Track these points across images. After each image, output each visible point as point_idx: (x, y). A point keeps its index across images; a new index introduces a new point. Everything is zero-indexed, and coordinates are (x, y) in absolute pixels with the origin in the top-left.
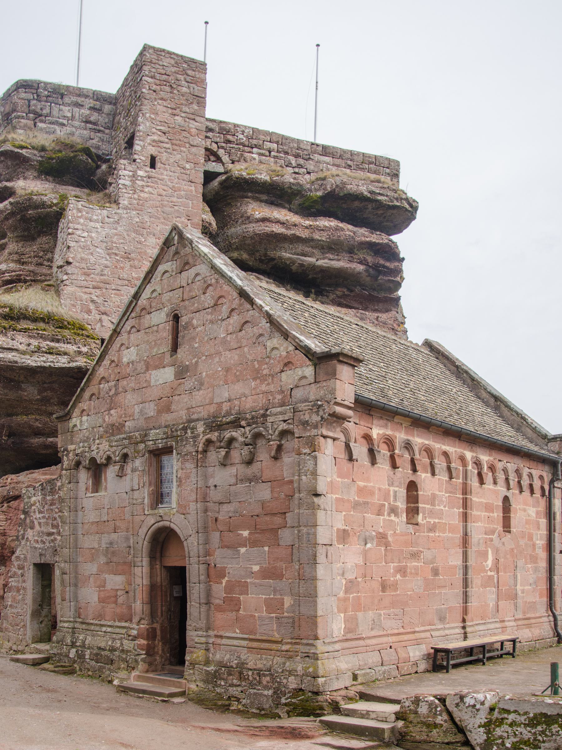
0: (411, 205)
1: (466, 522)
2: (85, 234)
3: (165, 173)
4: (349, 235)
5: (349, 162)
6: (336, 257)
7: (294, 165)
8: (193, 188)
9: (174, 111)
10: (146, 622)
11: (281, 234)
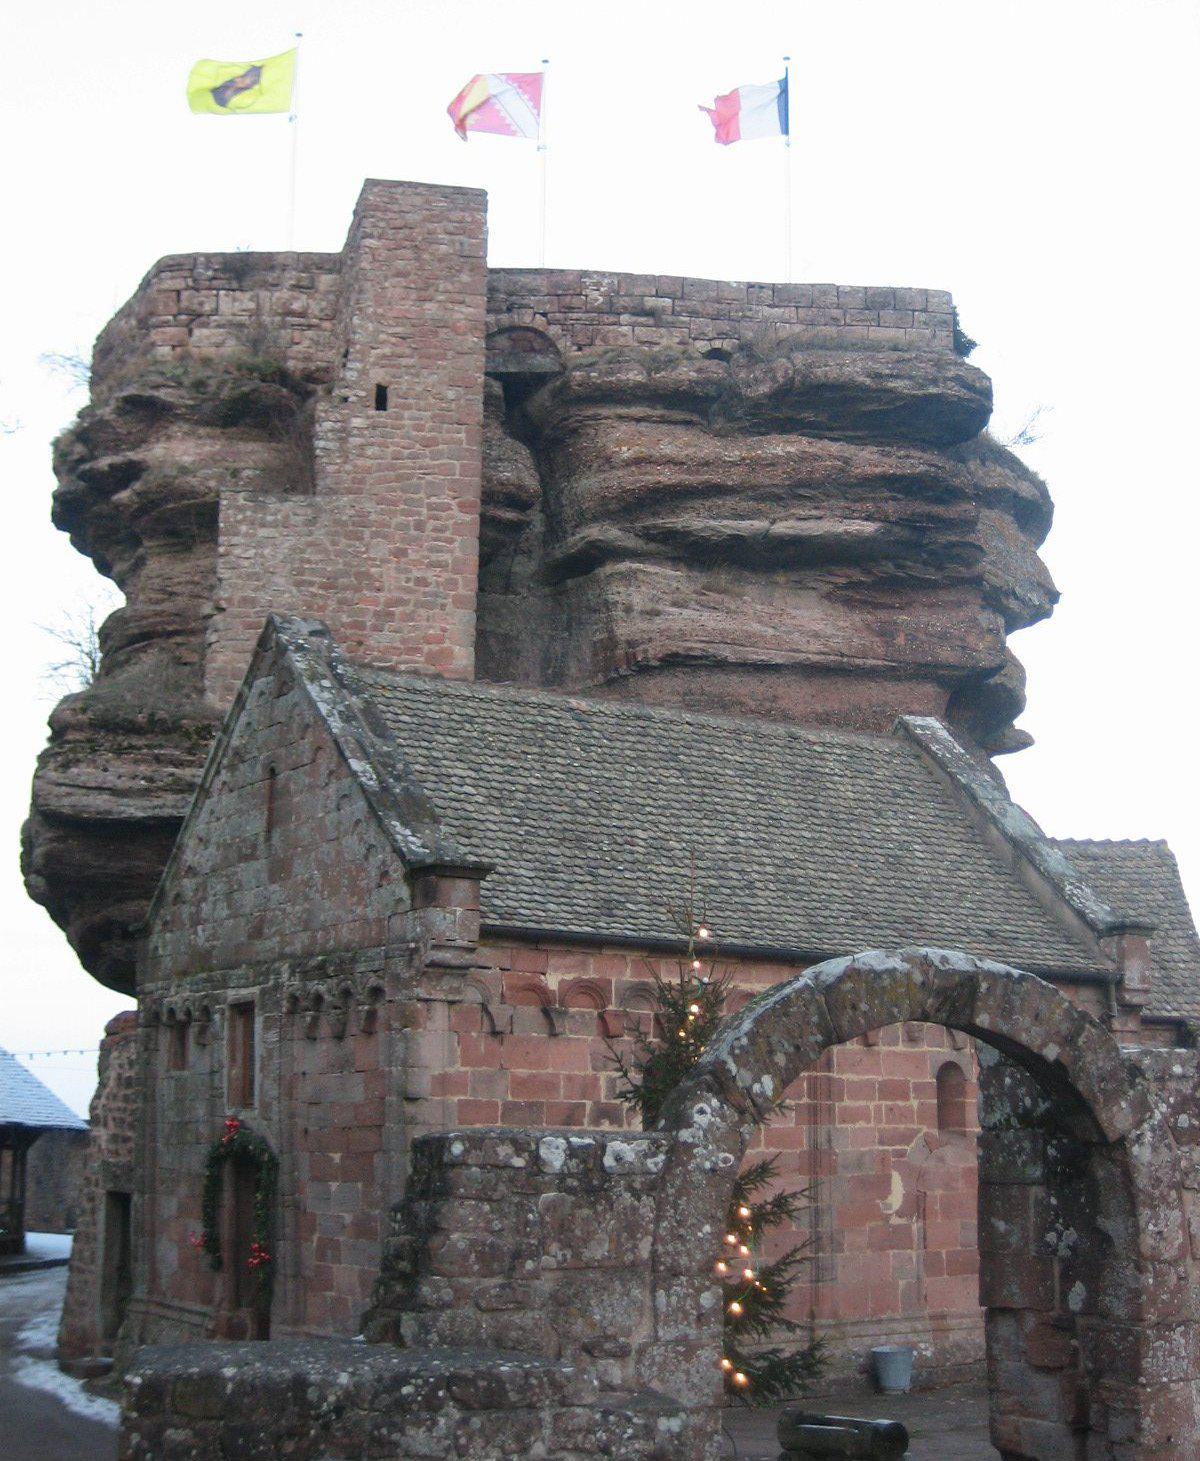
0: (970, 388)
1: (815, 1123)
3: (407, 414)
4: (833, 467)
5: (836, 313)
6: (814, 512)
7: (711, 335)
8: (462, 436)
9: (423, 293)
10: (807, 1278)
11: (679, 484)
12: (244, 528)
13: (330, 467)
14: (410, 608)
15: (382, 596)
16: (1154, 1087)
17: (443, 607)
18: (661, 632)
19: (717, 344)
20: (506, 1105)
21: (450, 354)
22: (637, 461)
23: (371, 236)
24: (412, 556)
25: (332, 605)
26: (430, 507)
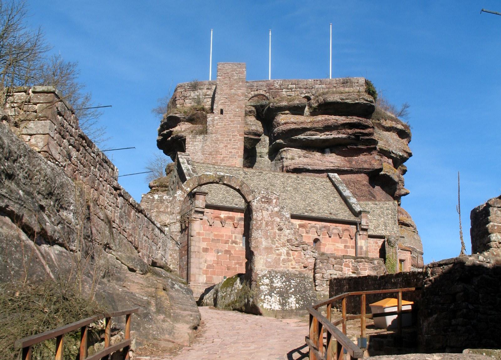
2: (193, 148)
3: (227, 115)
5: (335, 85)
8: (240, 119)
12: (191, 143)
13: (210, 129)
14: (228, 158)
15: (222, 156)
16: (257, 194)
17: (235, 158)
18: (293, 163)
19: (306, 95)
20: (212, 239)
21: (237, 101)
22: (285, 123)
23: (219, 76)
24: (229, 147)
25: (211, 158)
26: (233, 136)
